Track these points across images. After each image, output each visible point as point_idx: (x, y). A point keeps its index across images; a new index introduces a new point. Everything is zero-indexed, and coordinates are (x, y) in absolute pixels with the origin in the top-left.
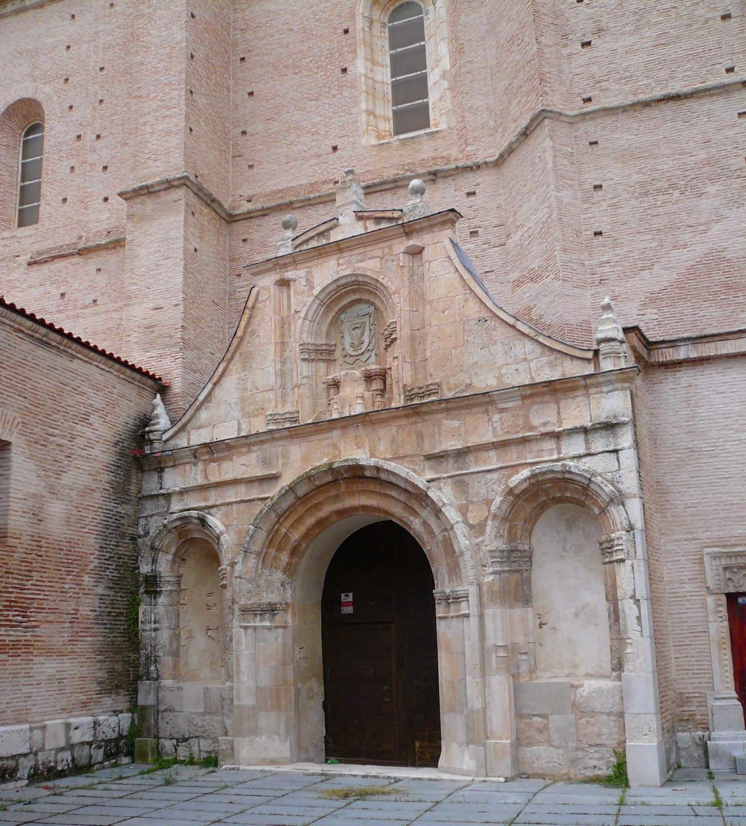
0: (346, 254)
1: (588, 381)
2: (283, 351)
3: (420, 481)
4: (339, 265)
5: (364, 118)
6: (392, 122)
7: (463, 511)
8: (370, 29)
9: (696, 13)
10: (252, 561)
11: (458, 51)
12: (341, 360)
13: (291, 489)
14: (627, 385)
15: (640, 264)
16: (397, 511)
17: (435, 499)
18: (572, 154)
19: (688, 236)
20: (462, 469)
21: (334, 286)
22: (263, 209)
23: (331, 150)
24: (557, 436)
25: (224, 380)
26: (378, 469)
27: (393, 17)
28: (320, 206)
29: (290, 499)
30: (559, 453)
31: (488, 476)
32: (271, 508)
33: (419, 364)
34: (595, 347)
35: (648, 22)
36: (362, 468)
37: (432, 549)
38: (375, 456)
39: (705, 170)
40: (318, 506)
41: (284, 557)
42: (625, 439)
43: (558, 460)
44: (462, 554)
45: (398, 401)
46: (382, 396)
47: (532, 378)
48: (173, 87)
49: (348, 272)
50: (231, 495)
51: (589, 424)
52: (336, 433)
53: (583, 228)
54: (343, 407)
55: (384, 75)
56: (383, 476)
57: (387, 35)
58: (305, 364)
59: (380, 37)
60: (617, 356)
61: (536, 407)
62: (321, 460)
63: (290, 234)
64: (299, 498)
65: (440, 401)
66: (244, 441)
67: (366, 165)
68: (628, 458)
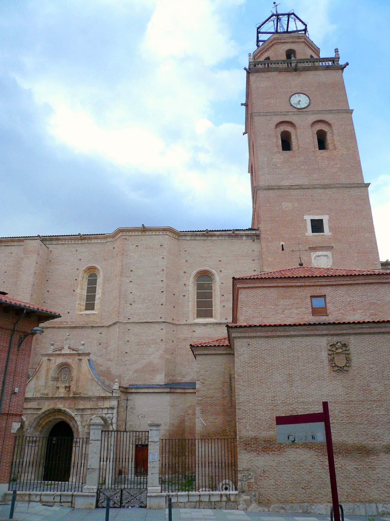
0: (65, 357)
1: (110, 397)
2: (47, 377)
3: (73, 414)
4: (63, 359)
5: (77, 306)
6: (85, 306)
7: (82, 422)
8: (83, 280)
9: (156, 302)
10: (32, 429)
11: (103, 293)
12: (60, 381)
13: (44, 412)
14: (117, 399)
15: (135, 362)
16: (67, 420)
17: (76, 419)
18: (123, 332)
19: (146, 357)
20: (82, 413)
21: (61, 364)
22: (47, 327)
23: (67, 313)
24: (102, 409)
25: (31, 381)
26: (65, 411)
27: (89, 277)
28: (63, 329)
29: (44, 415)
30: (102, 412)
31: (88, 415)
32: (39, 417)
33: (77, 387)
34: (112, 390)
35: (145, 302)
36: (61, 410)
37: (74, 430)
38: (65, 408)
39: (152, 341)
40: (50, 417)
41: (40, 429)
42: (115, 411)
43: (102, 414)
44: (80, 432)
45: (71, 395)
46: (68, 392)
47: (100, 395)
48: (27, 294)
49: (65, 361)
50: (29, 412)
51: (108, 407)
52: (56, 400)
53: (123, 351)
54: (59, 394)
55: (85, 293)
56: (65, 412)
57: (87, 281)
58: (51, 381)
59: (85, 282)
60: (116, 393)
61: (99, 401)
62: (52, 407)
63: (52, 347)
64: (46, 415)
65: (80, 397)
66: (34, 398)
67: (76, 319)
68: (115, 415)
